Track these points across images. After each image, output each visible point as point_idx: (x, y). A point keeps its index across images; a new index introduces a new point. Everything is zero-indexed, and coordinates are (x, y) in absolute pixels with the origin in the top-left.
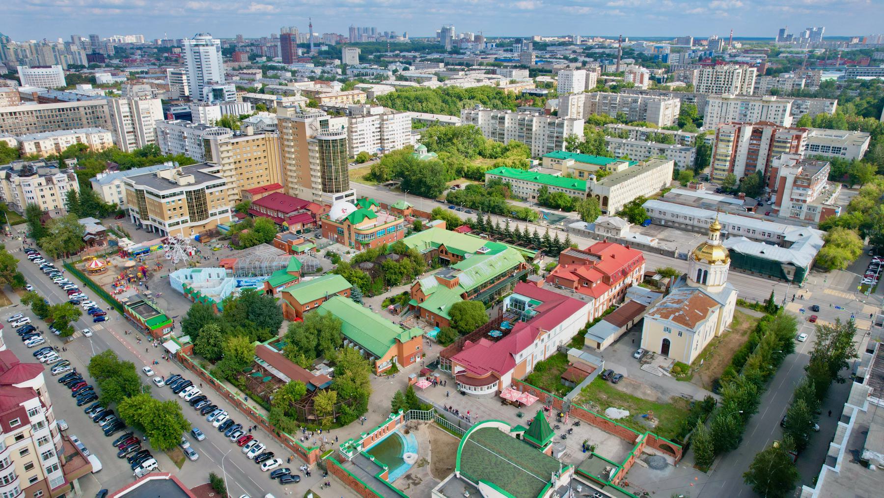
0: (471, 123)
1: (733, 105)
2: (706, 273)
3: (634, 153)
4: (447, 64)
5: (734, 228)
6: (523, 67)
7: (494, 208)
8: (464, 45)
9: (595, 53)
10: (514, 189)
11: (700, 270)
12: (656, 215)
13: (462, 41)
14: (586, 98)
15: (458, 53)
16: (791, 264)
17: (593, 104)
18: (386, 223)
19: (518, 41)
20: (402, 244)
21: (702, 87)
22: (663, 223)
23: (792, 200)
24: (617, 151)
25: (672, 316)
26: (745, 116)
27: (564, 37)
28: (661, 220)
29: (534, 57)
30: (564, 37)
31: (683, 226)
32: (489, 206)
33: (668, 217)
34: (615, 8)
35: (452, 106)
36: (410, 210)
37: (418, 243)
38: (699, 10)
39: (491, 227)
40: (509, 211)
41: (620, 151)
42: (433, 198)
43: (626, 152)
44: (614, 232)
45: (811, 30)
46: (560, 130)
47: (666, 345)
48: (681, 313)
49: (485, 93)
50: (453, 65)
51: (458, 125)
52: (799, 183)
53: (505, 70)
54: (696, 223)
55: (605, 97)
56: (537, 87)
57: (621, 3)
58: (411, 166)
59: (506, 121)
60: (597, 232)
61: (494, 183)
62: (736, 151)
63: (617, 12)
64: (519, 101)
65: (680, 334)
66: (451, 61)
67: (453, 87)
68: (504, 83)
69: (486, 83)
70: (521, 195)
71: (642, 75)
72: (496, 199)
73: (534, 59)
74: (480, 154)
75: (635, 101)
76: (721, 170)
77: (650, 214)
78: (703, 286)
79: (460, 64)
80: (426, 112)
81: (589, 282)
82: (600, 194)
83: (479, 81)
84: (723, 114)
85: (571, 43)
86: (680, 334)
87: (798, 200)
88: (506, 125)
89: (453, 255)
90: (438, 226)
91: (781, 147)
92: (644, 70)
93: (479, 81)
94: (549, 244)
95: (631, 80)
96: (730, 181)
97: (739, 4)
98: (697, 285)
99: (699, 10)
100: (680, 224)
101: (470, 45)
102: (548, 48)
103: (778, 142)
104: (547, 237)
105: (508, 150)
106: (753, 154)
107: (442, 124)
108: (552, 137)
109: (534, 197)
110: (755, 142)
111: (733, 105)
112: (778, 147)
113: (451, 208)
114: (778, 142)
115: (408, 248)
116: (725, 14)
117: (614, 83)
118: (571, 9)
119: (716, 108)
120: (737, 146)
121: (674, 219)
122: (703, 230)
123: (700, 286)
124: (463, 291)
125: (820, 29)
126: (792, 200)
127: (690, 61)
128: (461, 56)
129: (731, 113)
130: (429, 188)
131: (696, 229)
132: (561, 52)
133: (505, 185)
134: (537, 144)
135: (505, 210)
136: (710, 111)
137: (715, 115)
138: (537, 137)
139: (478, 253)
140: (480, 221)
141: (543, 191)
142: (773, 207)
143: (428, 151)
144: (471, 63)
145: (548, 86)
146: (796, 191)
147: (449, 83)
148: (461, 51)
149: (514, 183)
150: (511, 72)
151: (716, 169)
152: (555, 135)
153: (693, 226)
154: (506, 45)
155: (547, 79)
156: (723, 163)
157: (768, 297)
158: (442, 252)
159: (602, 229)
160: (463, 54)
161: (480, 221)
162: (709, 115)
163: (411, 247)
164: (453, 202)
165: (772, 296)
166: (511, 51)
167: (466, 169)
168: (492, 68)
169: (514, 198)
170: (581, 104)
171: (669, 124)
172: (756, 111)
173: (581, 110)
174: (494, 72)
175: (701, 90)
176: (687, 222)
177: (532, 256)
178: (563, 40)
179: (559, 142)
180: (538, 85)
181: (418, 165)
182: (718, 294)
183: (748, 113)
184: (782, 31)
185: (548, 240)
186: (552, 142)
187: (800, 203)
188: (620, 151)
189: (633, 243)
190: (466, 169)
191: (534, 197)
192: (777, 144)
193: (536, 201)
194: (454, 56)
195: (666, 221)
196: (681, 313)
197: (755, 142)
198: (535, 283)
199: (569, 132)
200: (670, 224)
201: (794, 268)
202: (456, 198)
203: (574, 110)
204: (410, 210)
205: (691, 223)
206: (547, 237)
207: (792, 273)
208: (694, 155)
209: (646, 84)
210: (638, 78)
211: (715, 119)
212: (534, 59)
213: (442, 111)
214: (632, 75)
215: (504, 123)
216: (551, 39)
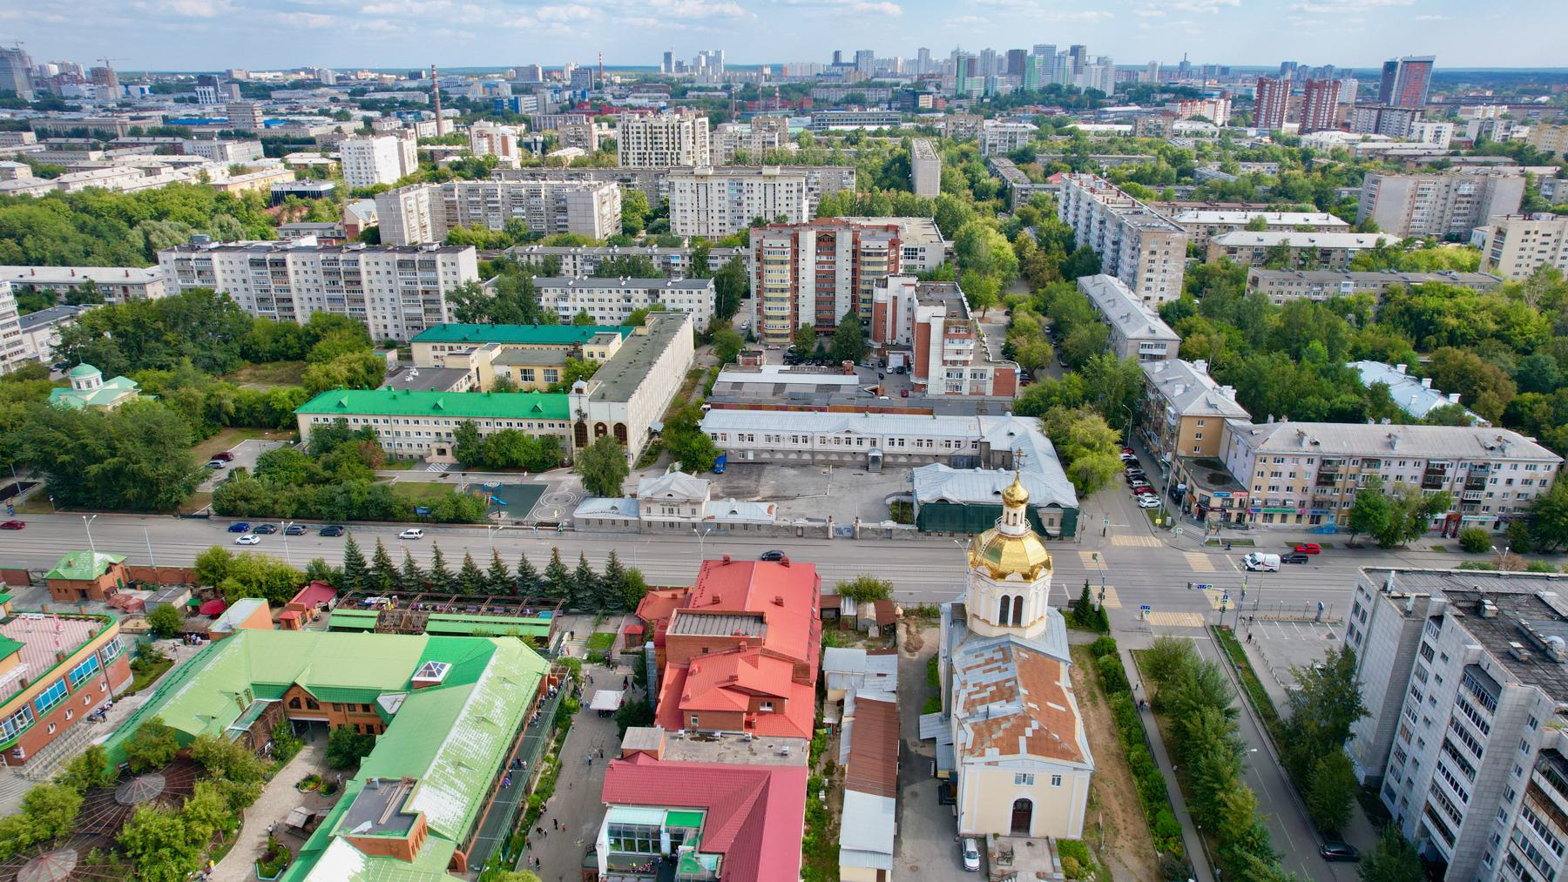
0: (197, 283)
1: (716, 188)
2: (1019, 600)
3: (596, 305)
4: (42, 135)
5: (892, 442)
6: (243, 136)
7: (364, 506)
8: (67, 90)
9: (377, 101)
10: (384, 439)
11: (1005, 600)
12: (732, 443)
13: (58, 79)
14: (432, 194)
15: (59, 107)
16: (1055, 505)
17: (451, 206)
18: (61, 658)
19: (205, 80)
20: (159, 729)
21: (631, 156)
22: (751, 457)
23: (945, 363)
24: (562, 304)
25: (1022, 741)
26: (740, 204)
27: (296, 72)
28: (743, 452)
29: (258, 113)
30: (296, 72)
31: (793, 456)
32: (350, 505)
33: (760, 443)
34: (374, 17)
35: (114, 242)
36: (117, 572)
37: (209, 696)
38: (524, 21)
39: (393, 574)
40: (406, 508)
41: (569, 304)
42: (170, 508)
43: (579, 305)
44: (686, 510)
45: (706, 53)
46: (431, 275)
47: (1022, 814)
48: (1035, 725)
49: (191, 201)
50: (58, 135)
51: (156, 292)
52: (952, 331)
53: (205, 143)
54: (818, 446)
55: (472, 191)
56: (300, 178)
57: (389, 8)
58: (72, 435)
59: (290, 268)
60: (645, 518)
61: (329, 439)
62: (796, 279)
63: (380, 24)
64: (277, 209)
65: (1057, 781)
66: (49, 126)
67: (95, 192)
68: (218, 174)
69: (168, 175)
70: (405, 450)
71: (504, 140)
72: (358, 485)
73: (261, 119)
74: (244, 355)
75: (535, 193)
76: (776, 318)
77: (719, 444)
78: (1014, 631)
79: (78, 133)
80: (40, 262)
81: (774, 700)
82: (605, 420)
83: (150, 171)
84: (703, 205)
85: (317, 84)
86: (1057, 781)
87: (954, 363)
88: (292, 277)
89: (336, 706)
90: (251, 623)
91: (874, 264)
92: (506, 129)
93: (150, 171)
94: (567, 585)
95: (486, 151)
96: (798, 333)
97: (892, 9)
98: (1002, 631)
99: (524, 21)
100: (786, 452)
101: (84, 89)
102: (274, 95)
103: (869, 254)
104: (556, 569)
105: (317, 338)
106: (825, 280)
107: (109, 289)
108: (415, 293)
109: (442, 452)
110: (824, 258)
111: (716, 188)
112: (869, 264)
113: (238, 529)
114: (869, 254)
115: (186, 739)
116: (567, 29)
117: (458, 159)
118: (292, 17)
119: (689, 195)
120: (797, 270)
121: (773, 445)
122: (834, 458)
123: (1010, 629)
124: (447, 852)
125: (718, 53)
126: (945, 363)
127: (557, 108)
128: (74, 115)
129: (716, 201)
130: (151, 485)
131: (820, 457)
132: (305, 99)
133: (359, 435)
134: (379, 312)
135: (397, 509)
136: (678, 201)
137: (689, 208)
138: (376, 295)
139: (412, 686)
140: (354, 561)
141: (467, 434)
142: (914, 380)
143: (106, 378)
144: (108, 130)
145: (321, 173)
146: (949, 346)
147: (76, 183)
148: (68, 103)
149: (382, 427)
150: (222, 148)
151: (770, 318)
152: (420, 287)
153: (813, 453)
154: (185, 89)
155: (312, 158)
156: (780, 305)
157: (1078, 596)
158: (296, 704)
159: (656, 509)
160: (78, 109)
161: (354, 561)
162: (678, 208)
163: (193, 728)
164: (237, 510)
165: (1086, 592)
166: (194, 101)
167: (231, 408)
168: (169, 140)
169: (394, 461)
170: (425, 208)
171: (611, 232)
172: (756, 195)
173: (427, 220)
174: (177, 150)
175: (631, 161)
176: (800, 446)
177: (544, 632)
178: (294, 77)
179: (433, 302)
180: (301, 172)
181: (96, 431)
182: (1039, 637)
183: (744, 198)
184: (668, 56)
185: (563, 577)
186: (416, 303)
187: (959, 366)
188: (569, 304)
189: (732, 526)
190: (231, 408)
191: (442, 452)
192: (867, 259)
193: (449, 458)
194: (53, 114)
195: (757, 452)
196: (1035, 725)
197: (824, 258)
198: (653, 755)
199: (451, 278)
200: (766, 456)
201: (1059, 511)
202: (247, 500)
203: (414, 223)
204: (117, 572)
205: (808, 446)
206: (556, 569)
207: (1057, 521)
208: (714, 295)
209: (515, 157)
210: (498, 146)
211: (689, 213)
212: (261, 119)
213: (88, 254)
214: (485, 141)
215: (285, 274)
216: (271, 76)
